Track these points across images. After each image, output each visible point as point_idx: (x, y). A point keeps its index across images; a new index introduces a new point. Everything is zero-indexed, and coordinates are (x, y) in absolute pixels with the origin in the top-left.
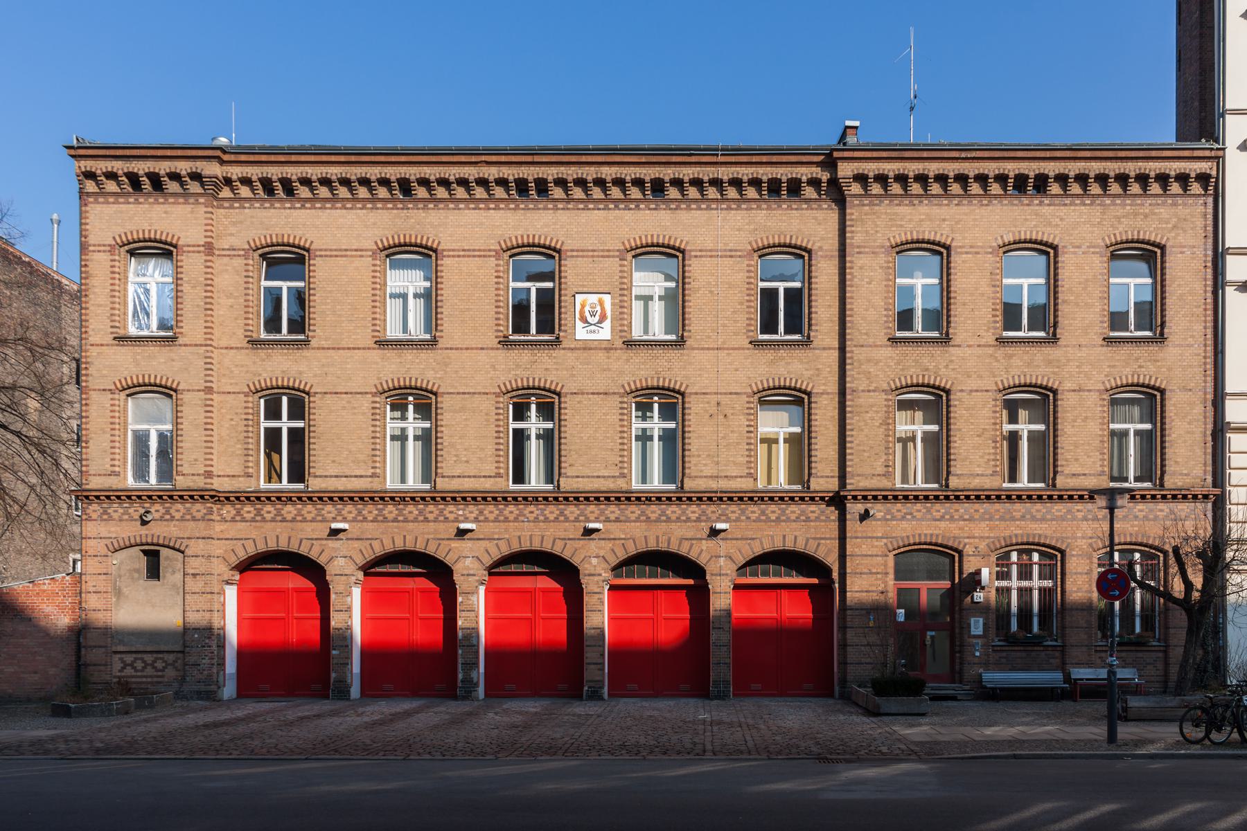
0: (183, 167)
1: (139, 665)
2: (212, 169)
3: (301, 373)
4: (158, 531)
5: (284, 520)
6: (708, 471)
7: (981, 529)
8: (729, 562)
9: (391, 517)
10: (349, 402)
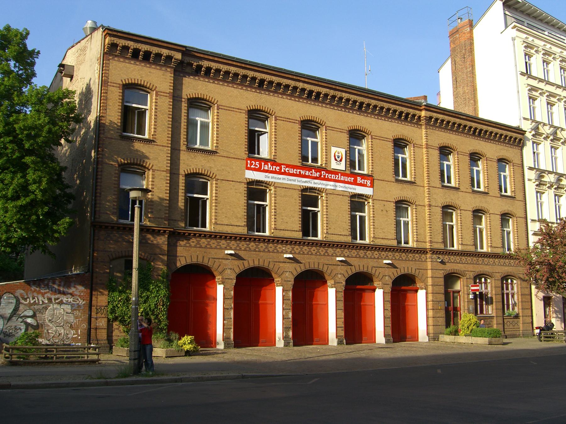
3: (211, 168)
5: (201, 247)
7: (470, 267)
8: (390, 279)
9: (252, 248)
10: (234, 186)
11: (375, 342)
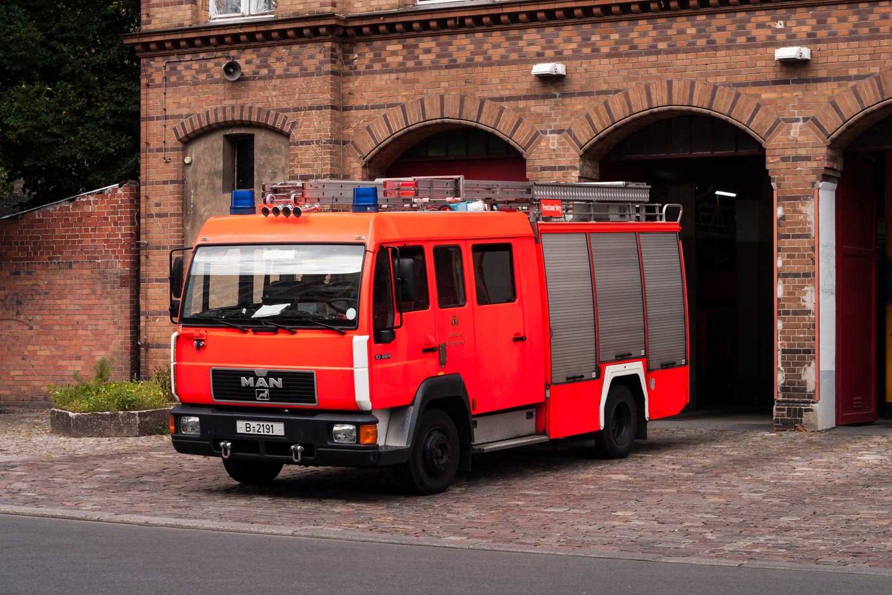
11: (645, 438)
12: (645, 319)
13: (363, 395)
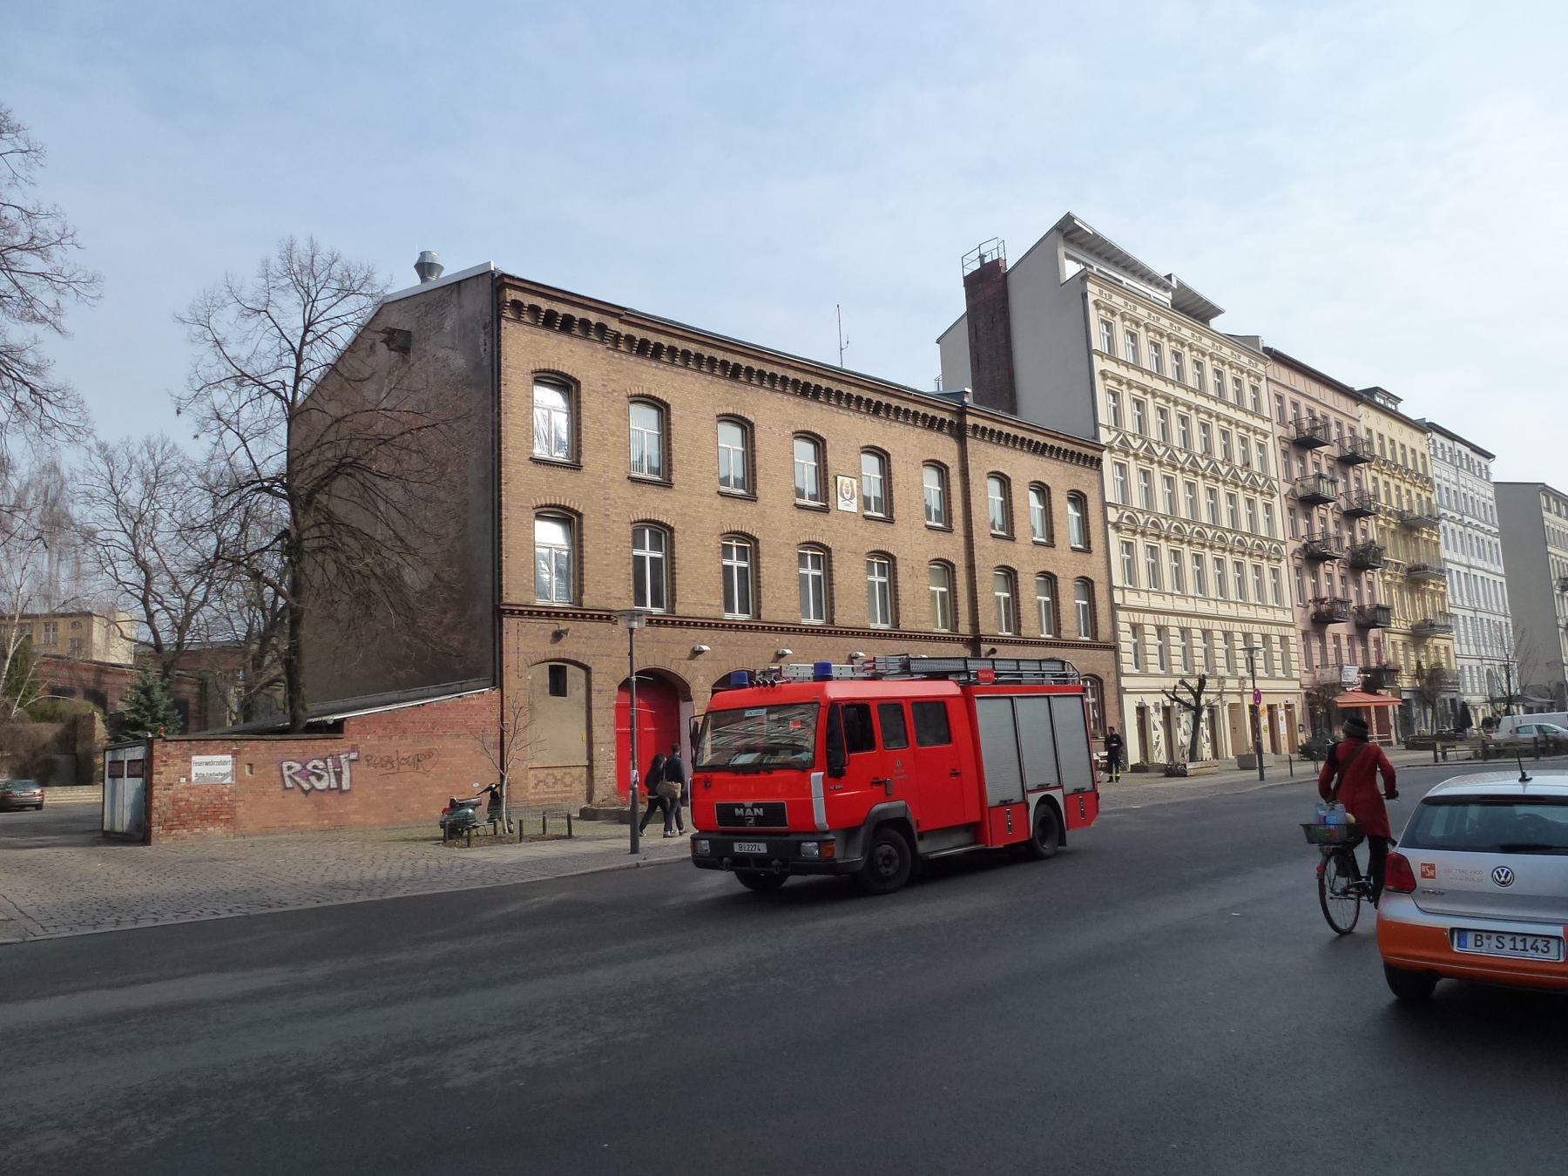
0: (594, 318)
1: (550, 780)
2: (614, 325)
4: (566, 649)
6: (693, 599)
12: (590, 757)
13: (820, 817)
